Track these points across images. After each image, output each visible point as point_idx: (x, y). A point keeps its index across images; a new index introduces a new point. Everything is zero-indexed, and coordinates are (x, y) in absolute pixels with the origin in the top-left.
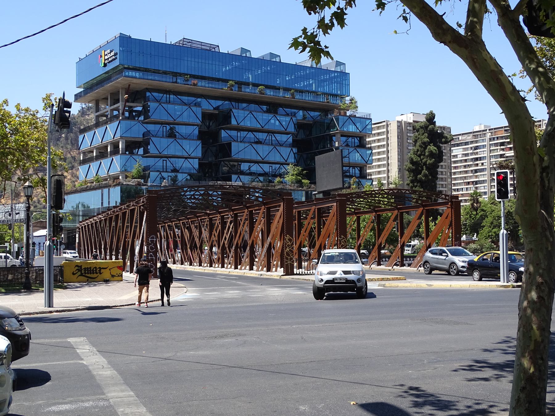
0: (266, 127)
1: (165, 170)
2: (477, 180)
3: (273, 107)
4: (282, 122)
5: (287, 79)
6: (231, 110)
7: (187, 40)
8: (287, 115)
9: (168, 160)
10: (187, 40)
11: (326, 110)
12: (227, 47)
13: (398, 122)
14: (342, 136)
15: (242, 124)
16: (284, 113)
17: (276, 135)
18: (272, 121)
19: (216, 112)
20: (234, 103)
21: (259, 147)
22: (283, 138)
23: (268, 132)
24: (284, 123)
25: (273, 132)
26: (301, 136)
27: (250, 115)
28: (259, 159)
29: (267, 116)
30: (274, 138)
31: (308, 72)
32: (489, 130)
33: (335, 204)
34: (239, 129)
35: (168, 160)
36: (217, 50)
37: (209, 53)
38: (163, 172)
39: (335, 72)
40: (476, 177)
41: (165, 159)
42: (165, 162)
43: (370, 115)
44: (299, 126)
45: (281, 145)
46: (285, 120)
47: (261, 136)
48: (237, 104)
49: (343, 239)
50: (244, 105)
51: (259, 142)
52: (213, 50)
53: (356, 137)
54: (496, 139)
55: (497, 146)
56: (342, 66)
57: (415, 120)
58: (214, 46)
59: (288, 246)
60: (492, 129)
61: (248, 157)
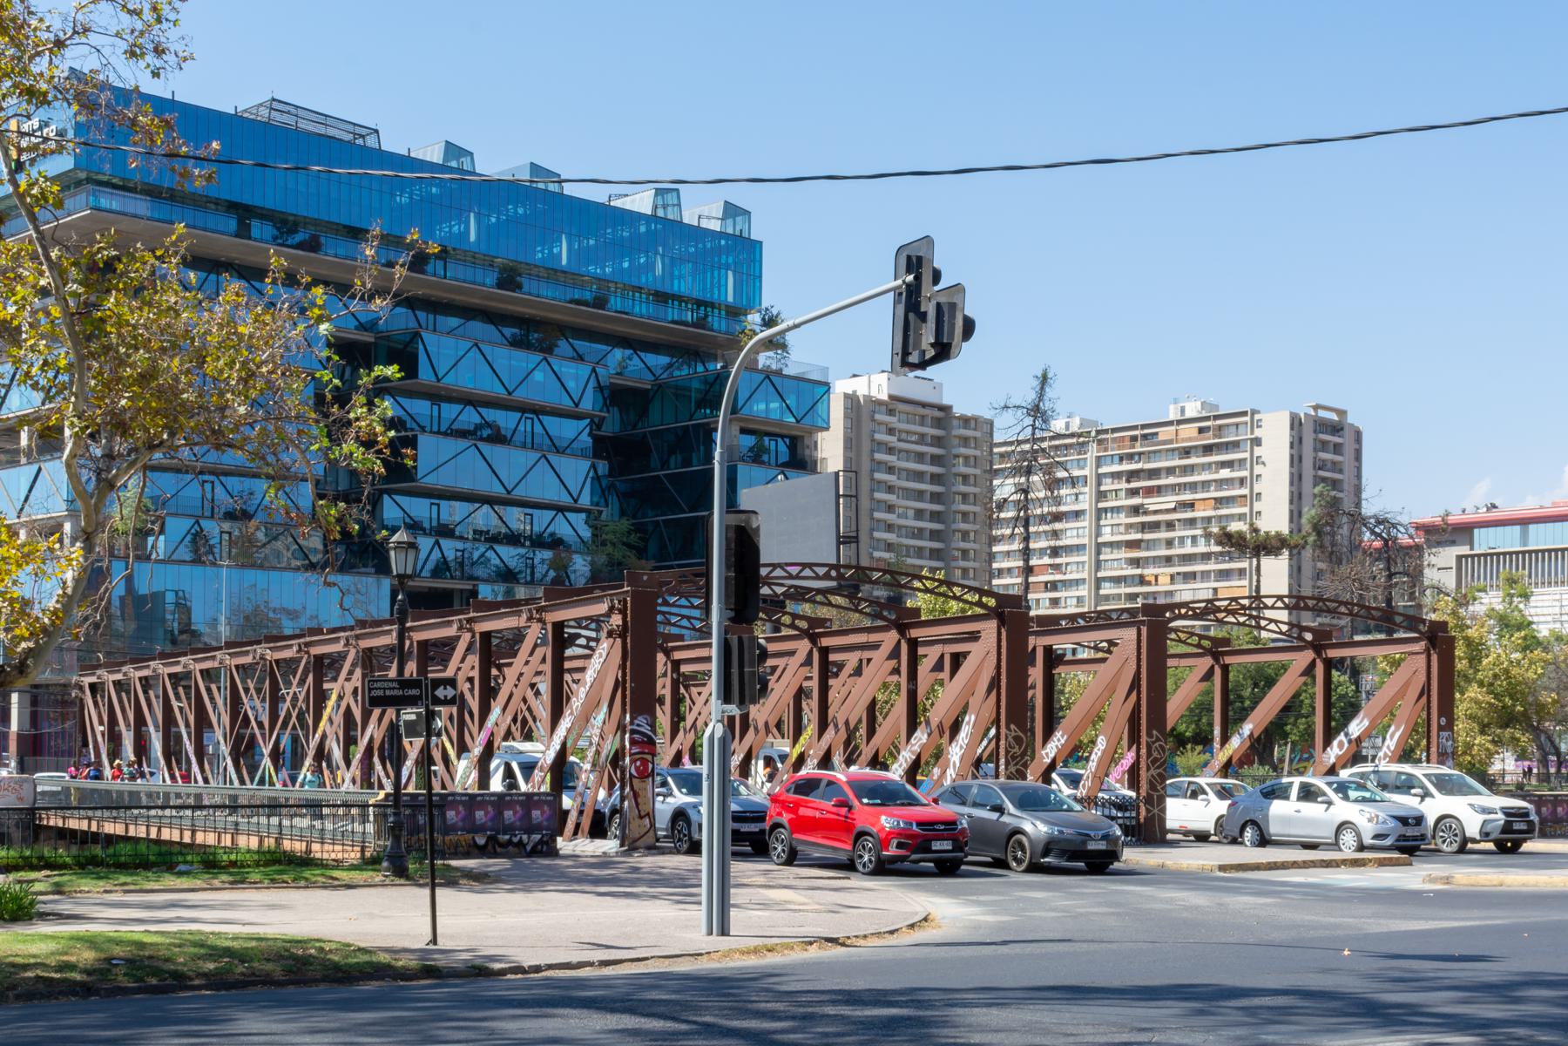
0: (521, 395)
1: (208, 513)
2: (1059, 577)
3: (535, 333)
4: (568, 379)
5: (592, 242)
6: (417, 335)
7: (280, 107)
8: (580, 358)
9: (217, 483)
10: (280, 107)
11: (690, 349)
12: (412, 134)
13: (846, 396)
14: (743, 431)
15: (449, 381)
16: (571, 353)
17: (546, 419)
18: (538, 376)
19: (368, 338)
20: (421, 315)
21: (494, 452)
22: (566, 430)
23: (526, 409)
24: (571, 385)
25: (537, 411)
26: (612, 426)
27: (474, 353)
28: (498, 490)
29: (524, 360)
30: (538, 428)
31: (643, 229)
32: (1098, 432)
33: (1130, 633)
34: (437, 396)
35: (217, 483)
36: (371, 142)
37: (351, 149)
38: (203, 517)
39: (722, 235)
40: (1057, 567)
41: (212, 478)
42: (208, 487)
43: (825, 370)
44: (617, 396)
45: (559, 451)
46: (575, 375)
47: (505, 420)
48: (431, 317)
49: (1158, 740)
50: (453, 322)
51: (498, 438)
52: (360, 142)
53: (782, 437)
54: (1116, 459)
55: (922, 482)
56: (739, 219)
57: (896, 393)
58: (364, 132)
59: (1013, 758)
60: (1106, 431)
61: (465, 485)
